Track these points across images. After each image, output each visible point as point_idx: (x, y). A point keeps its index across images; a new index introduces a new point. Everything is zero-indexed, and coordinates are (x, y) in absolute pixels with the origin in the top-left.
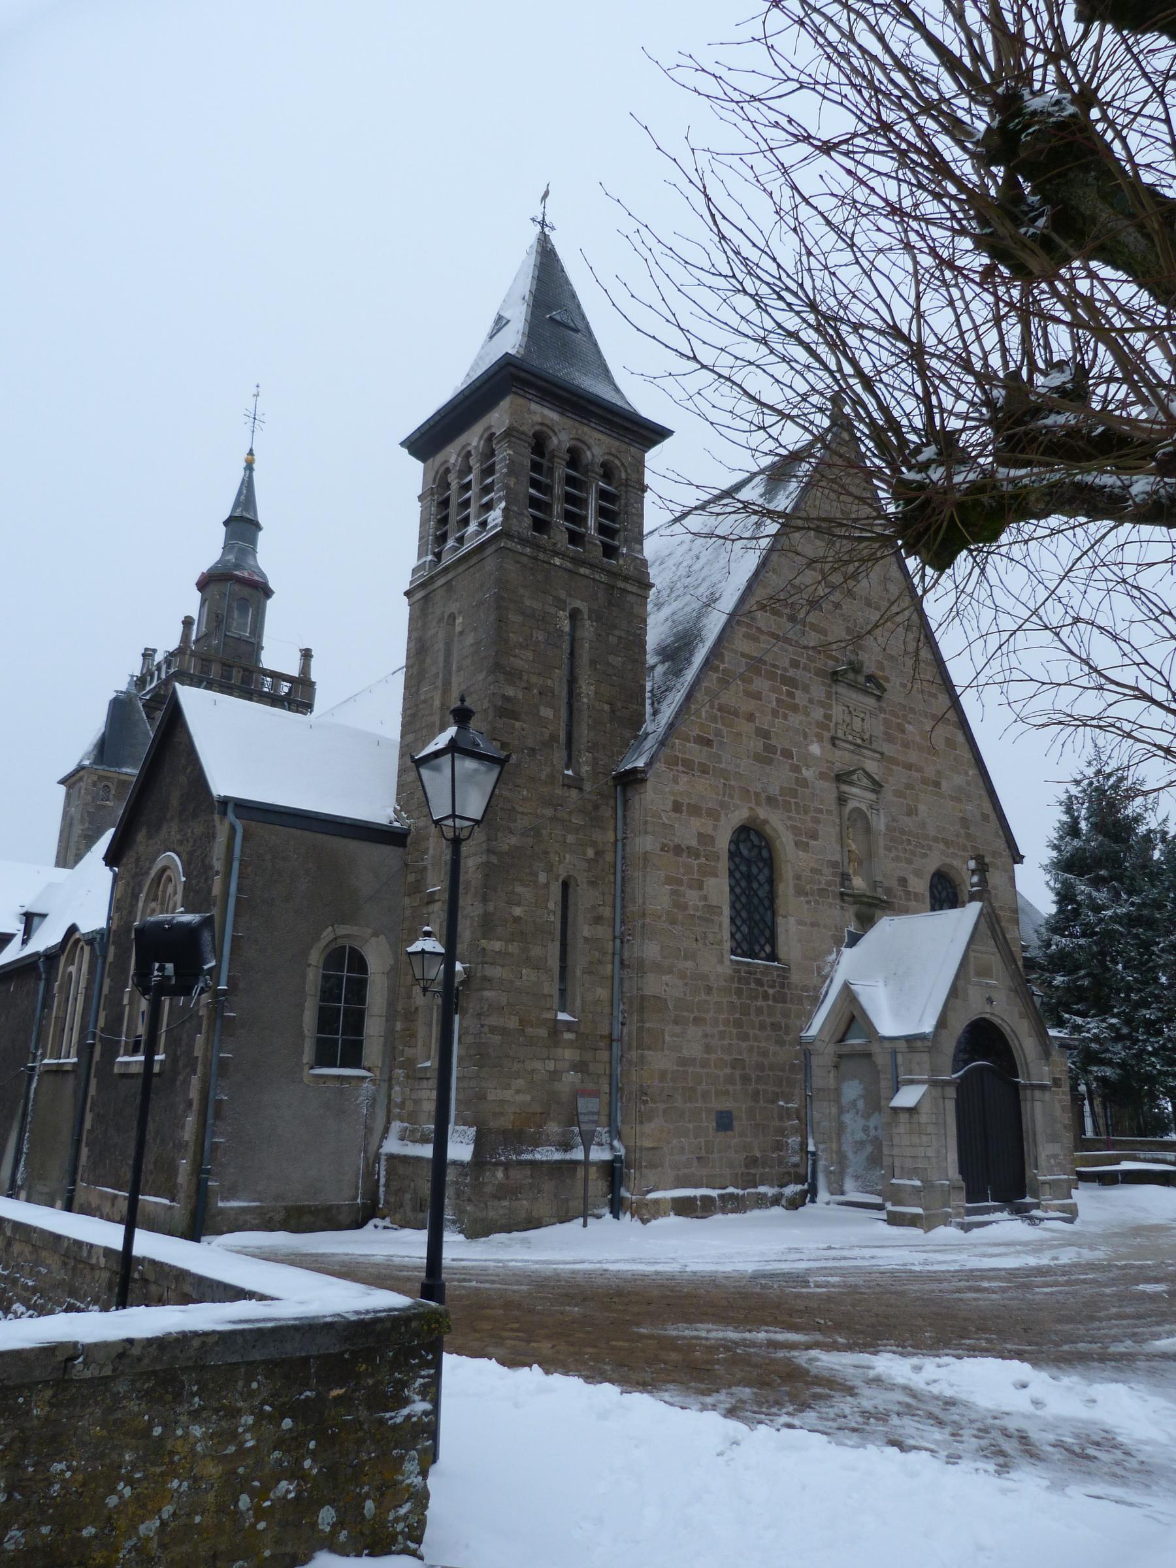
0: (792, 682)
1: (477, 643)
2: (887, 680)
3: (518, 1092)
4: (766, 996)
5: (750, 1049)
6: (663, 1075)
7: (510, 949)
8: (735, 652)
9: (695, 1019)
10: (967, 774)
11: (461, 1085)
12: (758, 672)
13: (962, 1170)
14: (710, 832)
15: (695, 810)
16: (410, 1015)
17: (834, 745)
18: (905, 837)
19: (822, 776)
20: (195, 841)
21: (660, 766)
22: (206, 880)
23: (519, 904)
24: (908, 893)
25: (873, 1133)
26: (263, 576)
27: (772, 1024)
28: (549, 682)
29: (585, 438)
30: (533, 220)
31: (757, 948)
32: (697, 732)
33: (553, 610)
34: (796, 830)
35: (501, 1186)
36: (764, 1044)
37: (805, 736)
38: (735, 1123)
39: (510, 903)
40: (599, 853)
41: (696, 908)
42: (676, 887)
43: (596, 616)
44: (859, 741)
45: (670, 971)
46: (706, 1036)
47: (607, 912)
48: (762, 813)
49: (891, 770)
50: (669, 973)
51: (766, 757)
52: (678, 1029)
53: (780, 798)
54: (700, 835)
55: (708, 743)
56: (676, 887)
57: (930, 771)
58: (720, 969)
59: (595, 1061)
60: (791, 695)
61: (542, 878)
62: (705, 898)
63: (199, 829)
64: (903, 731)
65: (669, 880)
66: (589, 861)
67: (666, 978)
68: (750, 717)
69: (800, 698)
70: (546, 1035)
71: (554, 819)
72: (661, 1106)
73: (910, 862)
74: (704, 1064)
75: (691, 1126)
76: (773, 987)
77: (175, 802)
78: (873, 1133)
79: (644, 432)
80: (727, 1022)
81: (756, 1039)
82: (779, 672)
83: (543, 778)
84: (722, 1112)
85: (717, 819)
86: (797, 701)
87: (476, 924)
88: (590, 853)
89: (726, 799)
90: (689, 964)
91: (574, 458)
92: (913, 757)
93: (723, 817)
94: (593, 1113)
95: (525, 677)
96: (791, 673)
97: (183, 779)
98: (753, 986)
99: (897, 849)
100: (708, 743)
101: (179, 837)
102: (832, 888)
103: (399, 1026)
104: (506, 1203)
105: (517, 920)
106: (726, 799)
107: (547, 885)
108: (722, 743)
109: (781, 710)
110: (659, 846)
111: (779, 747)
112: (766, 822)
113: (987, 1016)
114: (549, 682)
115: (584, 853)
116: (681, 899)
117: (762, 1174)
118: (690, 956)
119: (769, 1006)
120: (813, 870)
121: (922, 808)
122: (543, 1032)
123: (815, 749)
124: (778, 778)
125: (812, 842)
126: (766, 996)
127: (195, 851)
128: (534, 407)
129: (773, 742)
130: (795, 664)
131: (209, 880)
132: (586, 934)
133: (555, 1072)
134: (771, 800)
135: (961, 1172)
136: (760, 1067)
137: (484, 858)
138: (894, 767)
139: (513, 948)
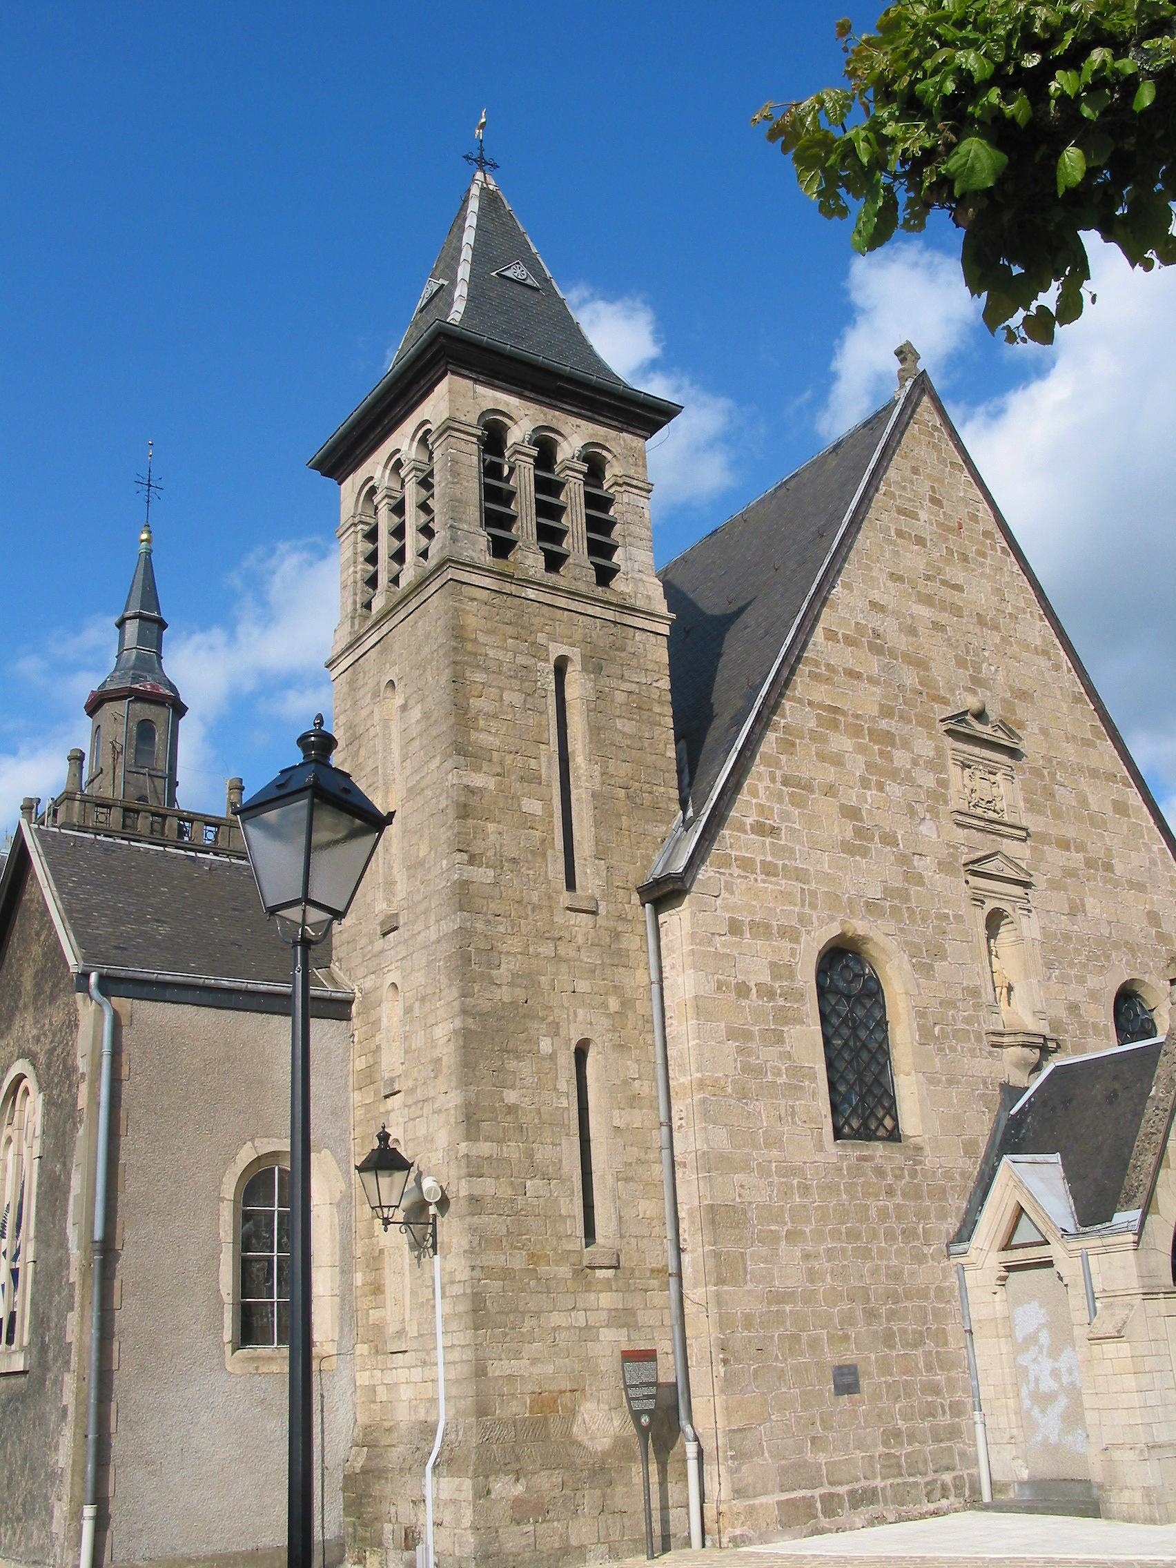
0: (886, 738)
1: (426, 715)
2: (1021, 725)
3: (534, 1361)
5: (874, 1272)
11: (451, 1358)
12: (834, 725)
15: (762, 929)
16: (375, 1260)
20: (54, 1035)
22: (70, 1086)
23: (513, 1087)
24: (1083, 1026)
25: (1066, 1379)
26: (173, 688)
28: (533, 763)
29: (554, 425)
30: (467, 158)
34: (913, 950)
38: (864, 1383)
40: (626, 1004)
43: (595, 666)
45: (746, 1167)
46: (807, 1256)
47: (643, 1088)
48: (860, 926)
54: (773, 965)
55: (774, 831)
58: (819, 1157)
61: (546, 1045)
63: (58, 1017)
64: (1052, 795)
67: (739, 1177)
68: (830, 791)
73: (1081, 980)
74: (809, 1298)
77: (28, 984)
78: (1066, 1379)
81: (882, 1253)
84: (840, 1368)
85: (796, 940)
87: (453, 1120)
88: (614, 1004)
89: (807, 910)
90: (775, 1153)
92: (1070, 832)
96: (884, 724)
97: (36, 950)
100: (774, 831)
101: (35, 1032)
103: (359, 1278)
105: (512, 1109)
106: (807, 910)
107: (553, 1057)
108: (791, 830)
110: (714, 985)
112: (865, 939)
113: (112, 1463)
114: (533, 763)
115: (604, 1005)
116: (752, 1060)
117: (908, 1455)
118: (774, 1141)
119: (897, 1206)
121: (1090, 902)
127: (54, 1049)
128: (481, 389)
129: (867, 824)
130: (886, 712)
131: (73, 1086)
136: (892, 1296)
137: (458, 1023)
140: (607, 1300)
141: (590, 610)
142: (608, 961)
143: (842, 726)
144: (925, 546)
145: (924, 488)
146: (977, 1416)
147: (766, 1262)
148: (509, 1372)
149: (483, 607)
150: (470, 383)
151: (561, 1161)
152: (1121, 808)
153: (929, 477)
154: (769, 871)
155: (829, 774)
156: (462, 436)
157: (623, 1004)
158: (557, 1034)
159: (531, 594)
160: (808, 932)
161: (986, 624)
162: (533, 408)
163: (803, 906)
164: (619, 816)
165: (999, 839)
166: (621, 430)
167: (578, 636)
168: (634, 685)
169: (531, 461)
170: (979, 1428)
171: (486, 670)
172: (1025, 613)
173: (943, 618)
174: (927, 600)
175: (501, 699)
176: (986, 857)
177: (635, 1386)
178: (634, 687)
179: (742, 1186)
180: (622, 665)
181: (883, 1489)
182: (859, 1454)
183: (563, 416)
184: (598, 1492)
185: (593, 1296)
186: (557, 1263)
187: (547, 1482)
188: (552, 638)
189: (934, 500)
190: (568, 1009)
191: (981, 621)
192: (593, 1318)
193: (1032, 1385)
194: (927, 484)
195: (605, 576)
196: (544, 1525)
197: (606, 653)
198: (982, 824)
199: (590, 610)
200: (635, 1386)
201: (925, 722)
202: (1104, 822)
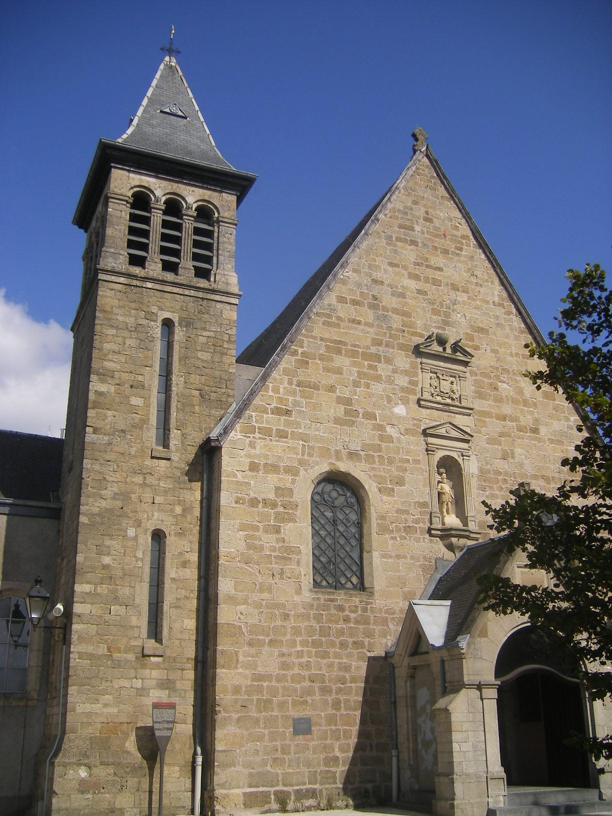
4: (347, 620)
6: (237, 690)
7: (99, 590)
8: (315, 338)
9: (271, 641)
10: (568, 420)
12: (339, 352)
13: (504, 762)
14: (288, 485)
15: (273, 468)
17: (420, 406)
18: (500, 478)
19: (408, 431)
21: (235, 435)
23: (108, 554)
27: (355, 643)
28: (140, 378)
29: (178, 192)
30: (162, 49)
31: (343, 581)
32: (274, 405)
33: (145, 322)
35: (82, 782)
36: (345, 660)
37: (389, 400)
39: (100, 553)
41: (273, 549)
42: (251, 533)
44: (449, 401)
45: (245, 602)
49: (484, 422)
50: (243, 604)
51: (349, 417)
52: (253, 651)
53: (362, 453)
54: (277, 489)
55: (288, 413)
56: (251, 533)
57: (527, 420)
58: (297, 598)
59: (182, 679)
60: (375, 368)
61: (131, 532)
62: (283, 540)
64: (496, 389)
65: (243, 527)
66: (176, 516)
67: (242, 608)
68: (331, 389)
69: (383, 369)
70: (134, 659)
71: (144, 485)
72: (235, 716)
75: (266, 732)
76: (356, 611)
79: (229, 179)
80: (304, 643)
82: (360, 350)
83: (133, 453)
86: (379, 372)
88: (178, 510)
90: (266, 595)
91: (173, 207)
92: (507, 409)
93: (302, 472)
94: (168, 722)
95: (117, 375)
96: (373, 350)
98: (333, 611)
99: (491, 488)
100: (288, 413)
102: (421, 525)
104: (90, 796)
105: (105, 567)
107: (136, 538)
109: (363, 381)
111: (361, 411)
114: (140, 378)
115: (172, 511)
116: (257, 542)
120: (399, 511)
121: (518, 451)
122: (131, 657)
123: (400, 410)
124: (360, 436)
125: (397, 488)
126: (347, 620)
128: (132, 175)
132: (173, 575)
133: (143, 689)
134: (353, 455)
135: (503, 764)
138: (487, 419)
139: (103, 589)
140: (155, 674)
141: (187, 292)
142: (178, 486)
143: (343, 352)
144: (417, 246)
145: (420, 211)
146: (394, 752)
147: (253, 657)
148: (89, 710)
149: (119, 293)
150: (126, 173)
151: (134, 596)
152: (186, 405)
153: (425, 206)
154: (282, 435)
155: (332, 379)
156: (117, 201)
157: (184, 510)
158: (139, 526)
159: (149, 285)
160: (306, 470)
161: (458, 290)
162: (164, 183)
163: (303, 455)
164: (193, 406)
165: (453, 415)
166: (221, 192)
167: (178, 307)
168: (212, 333)
169: (161, 212)
170: (394, 760)
171: (117, 328)
172: (488, 282)
173: (427, 287)
174: (416, 277)
175: (124, 343)
176: (438, 426)
177: (159, 722)
178: (212, 334)
179: (241, 613)
180: (205, 322)
181: (321, 791)
182: (306, 770)
183: (183, 186)
184: (136, 780)
185: (148, 671)
186: (125, 652)
187: (102, 772)
188: (161, 309)
189: (427, 219)
190: (147, 512)
191: (455, 288)
192: (148, 683)
193: (423, 736)
194: (423, 210)
195: (203, 274)
196: (99, 795)
197: (195, 315)
198: (440, 406)
199: (187, 292)
200: (159, 722)
201: (402, 347)
202: (535, 404)
